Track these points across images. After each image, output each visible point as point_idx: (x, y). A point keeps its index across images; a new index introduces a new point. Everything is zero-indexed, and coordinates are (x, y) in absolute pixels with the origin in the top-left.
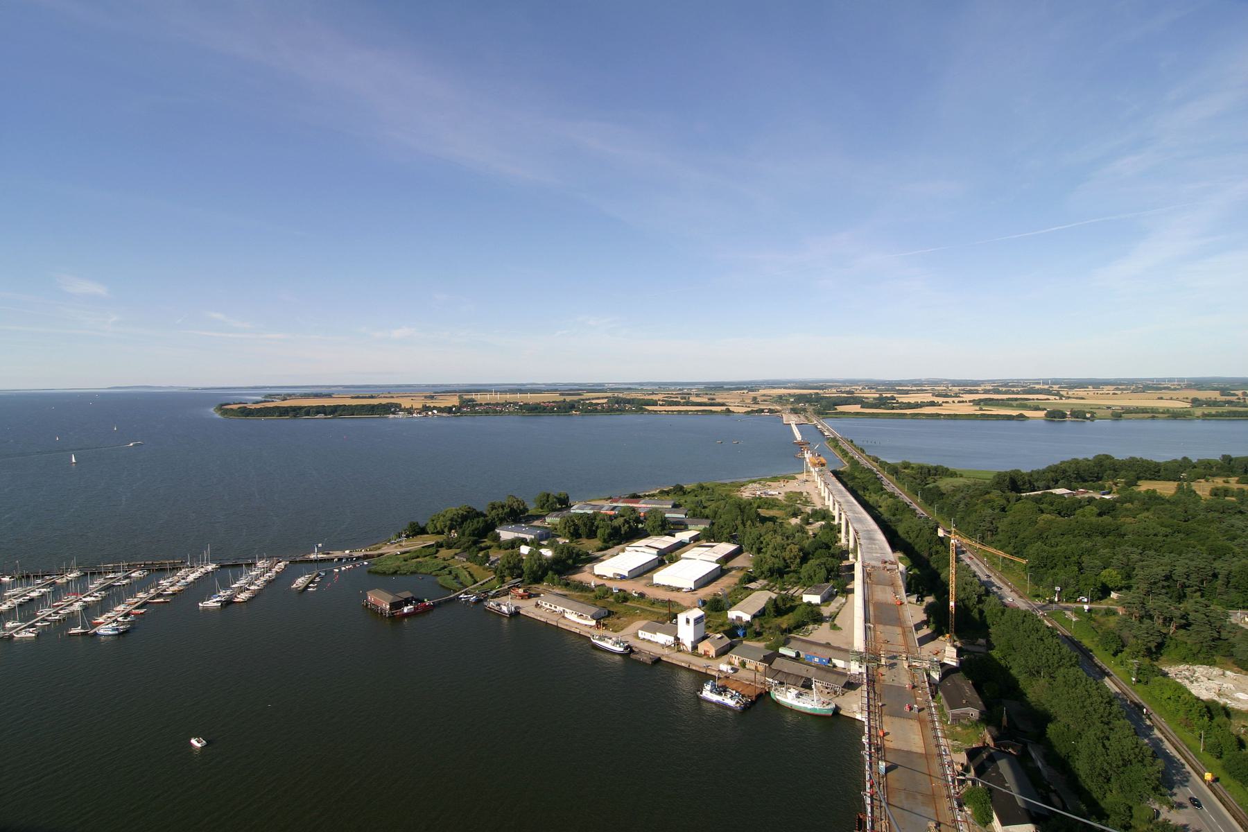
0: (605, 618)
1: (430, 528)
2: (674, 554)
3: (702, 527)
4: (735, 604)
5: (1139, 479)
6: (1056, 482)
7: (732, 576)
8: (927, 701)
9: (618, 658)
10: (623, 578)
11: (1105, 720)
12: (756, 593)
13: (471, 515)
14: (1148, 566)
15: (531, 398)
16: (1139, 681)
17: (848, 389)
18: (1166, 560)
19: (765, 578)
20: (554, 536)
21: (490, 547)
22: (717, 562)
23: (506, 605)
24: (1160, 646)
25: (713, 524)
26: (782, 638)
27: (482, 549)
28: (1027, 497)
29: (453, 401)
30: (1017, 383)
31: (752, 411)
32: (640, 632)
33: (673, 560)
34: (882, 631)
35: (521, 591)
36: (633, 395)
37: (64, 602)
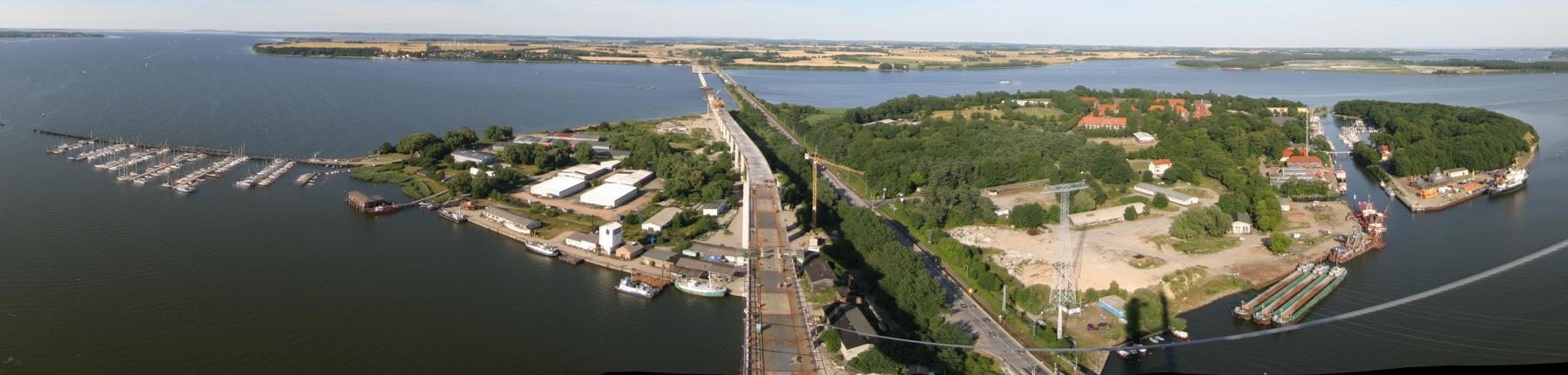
0: (538, 228)
1: (399, 149)
2: (598, 179)
3: (623, 157)
4: (648, 218)
5: (933, 110)
6: (885, 114)
7: (647, 196)
8: (794, 279)
9: (548, 259)
10: (555, 197)
11: (913, 271)
12: (666, 209)
13: (431, 141)
14: (938, 168)
15: (485, 47)
16: (933, 243)
17: (744, 45)
18: (947, 163)
19: (673, 197)
20: (499, 161)
21: (446, 167)
22: (635, 185)
23: (457, 214)
24: (945, 218)
25: (632, 155)
26: (686, 243)
27: (439, 168)
28: (866, 127)
29: (422, 48)
30: (861, 44)
31: (668, 62)
32: (567, 240)
33: (597, 184)
35: (469, 203)
37: (160, 166)
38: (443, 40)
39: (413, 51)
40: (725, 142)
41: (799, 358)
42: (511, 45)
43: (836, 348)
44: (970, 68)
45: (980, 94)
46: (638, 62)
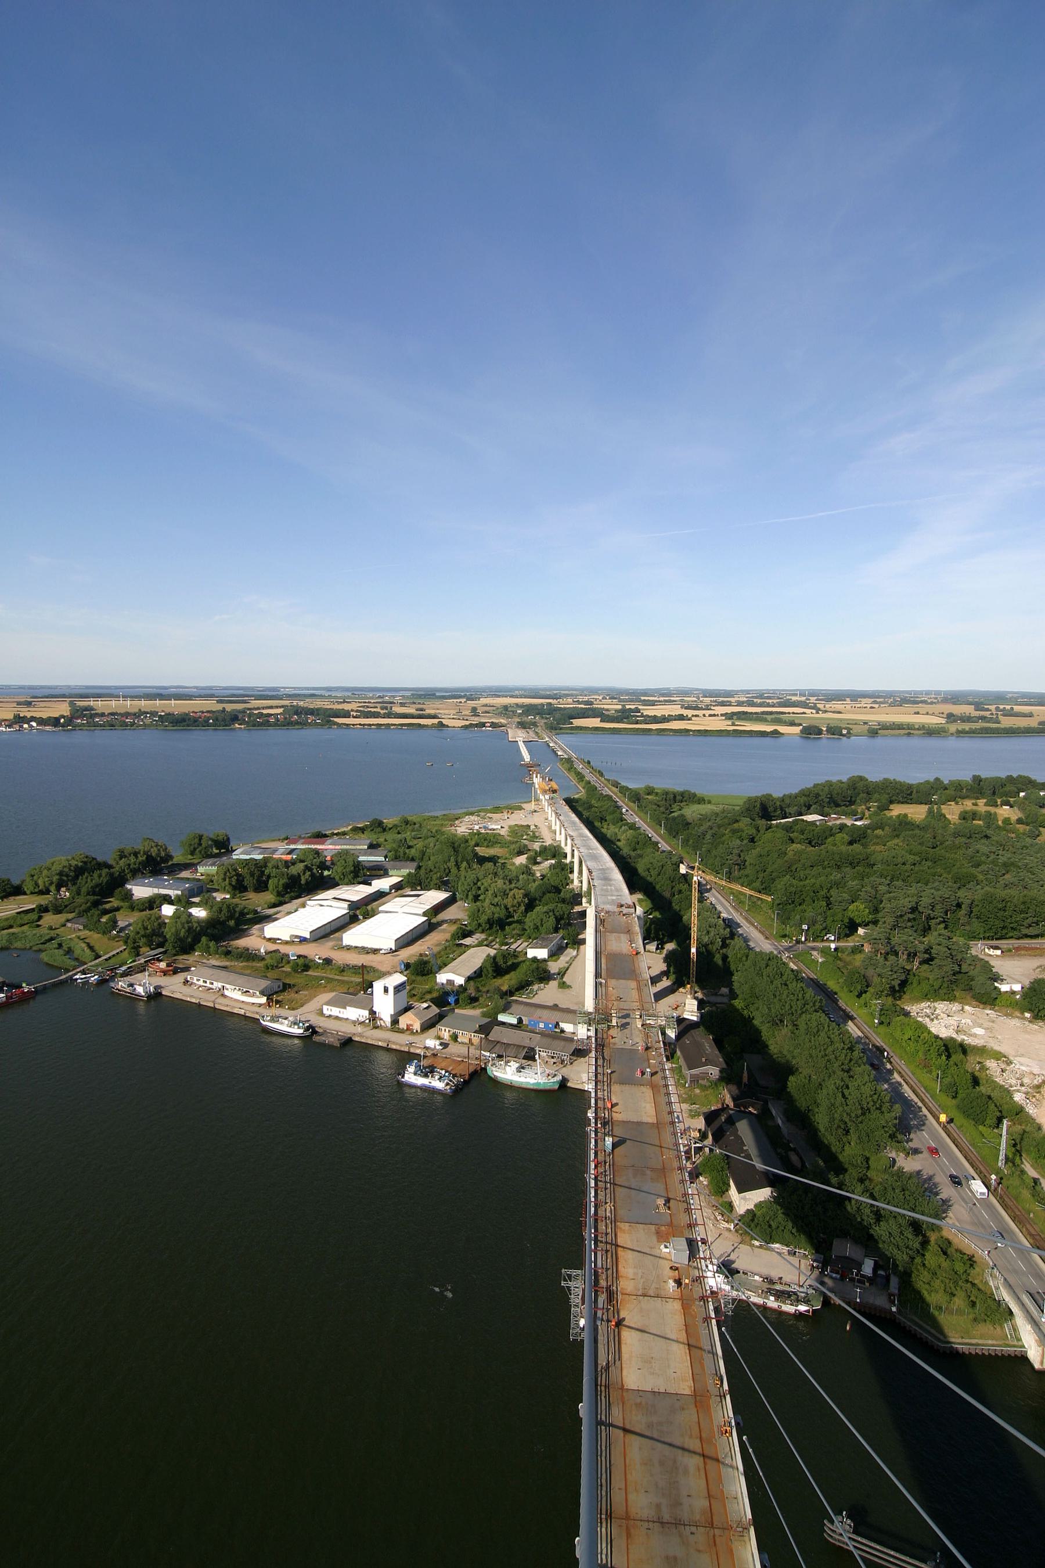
1: (28, 887)
2: (369, 908)
3: (405, 872)
5: (891, 802)
6: (809, 807)
7: (444, 931)
9: (296, 1041)
10: (303, 940)
11: (846, 1067)
12: (472, 950)
13: (88, 866)
14: (895, 898)
16: (881, 1023)
18: (913, 891)
19: (483, 932)
21: (117, 909)
22: (424, 914)
23: (142, 985)
24: (904, 984)
25: (419, 867)
26: (502, 1002)
27: (106, 912)
28: (777, 825)
29: (62, 709)
30: (773, 694)
32: (325, 1007)
33: (368, 915)
34: (616, 986)
35: (163, 965)
36: (318, 704)
38: (99, 696)
39: (45, 716)
40: (559, 846)
41: (668, 1201)
42: (218, 702)
43: (721, 1190)
44: (960, 733)
45: (977, 780)
46: (424, 726)
